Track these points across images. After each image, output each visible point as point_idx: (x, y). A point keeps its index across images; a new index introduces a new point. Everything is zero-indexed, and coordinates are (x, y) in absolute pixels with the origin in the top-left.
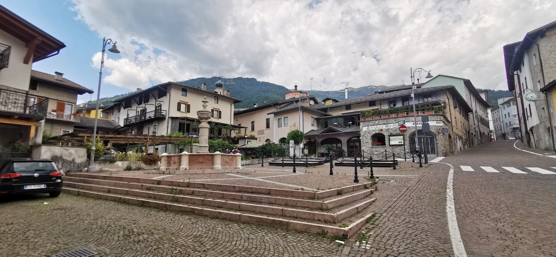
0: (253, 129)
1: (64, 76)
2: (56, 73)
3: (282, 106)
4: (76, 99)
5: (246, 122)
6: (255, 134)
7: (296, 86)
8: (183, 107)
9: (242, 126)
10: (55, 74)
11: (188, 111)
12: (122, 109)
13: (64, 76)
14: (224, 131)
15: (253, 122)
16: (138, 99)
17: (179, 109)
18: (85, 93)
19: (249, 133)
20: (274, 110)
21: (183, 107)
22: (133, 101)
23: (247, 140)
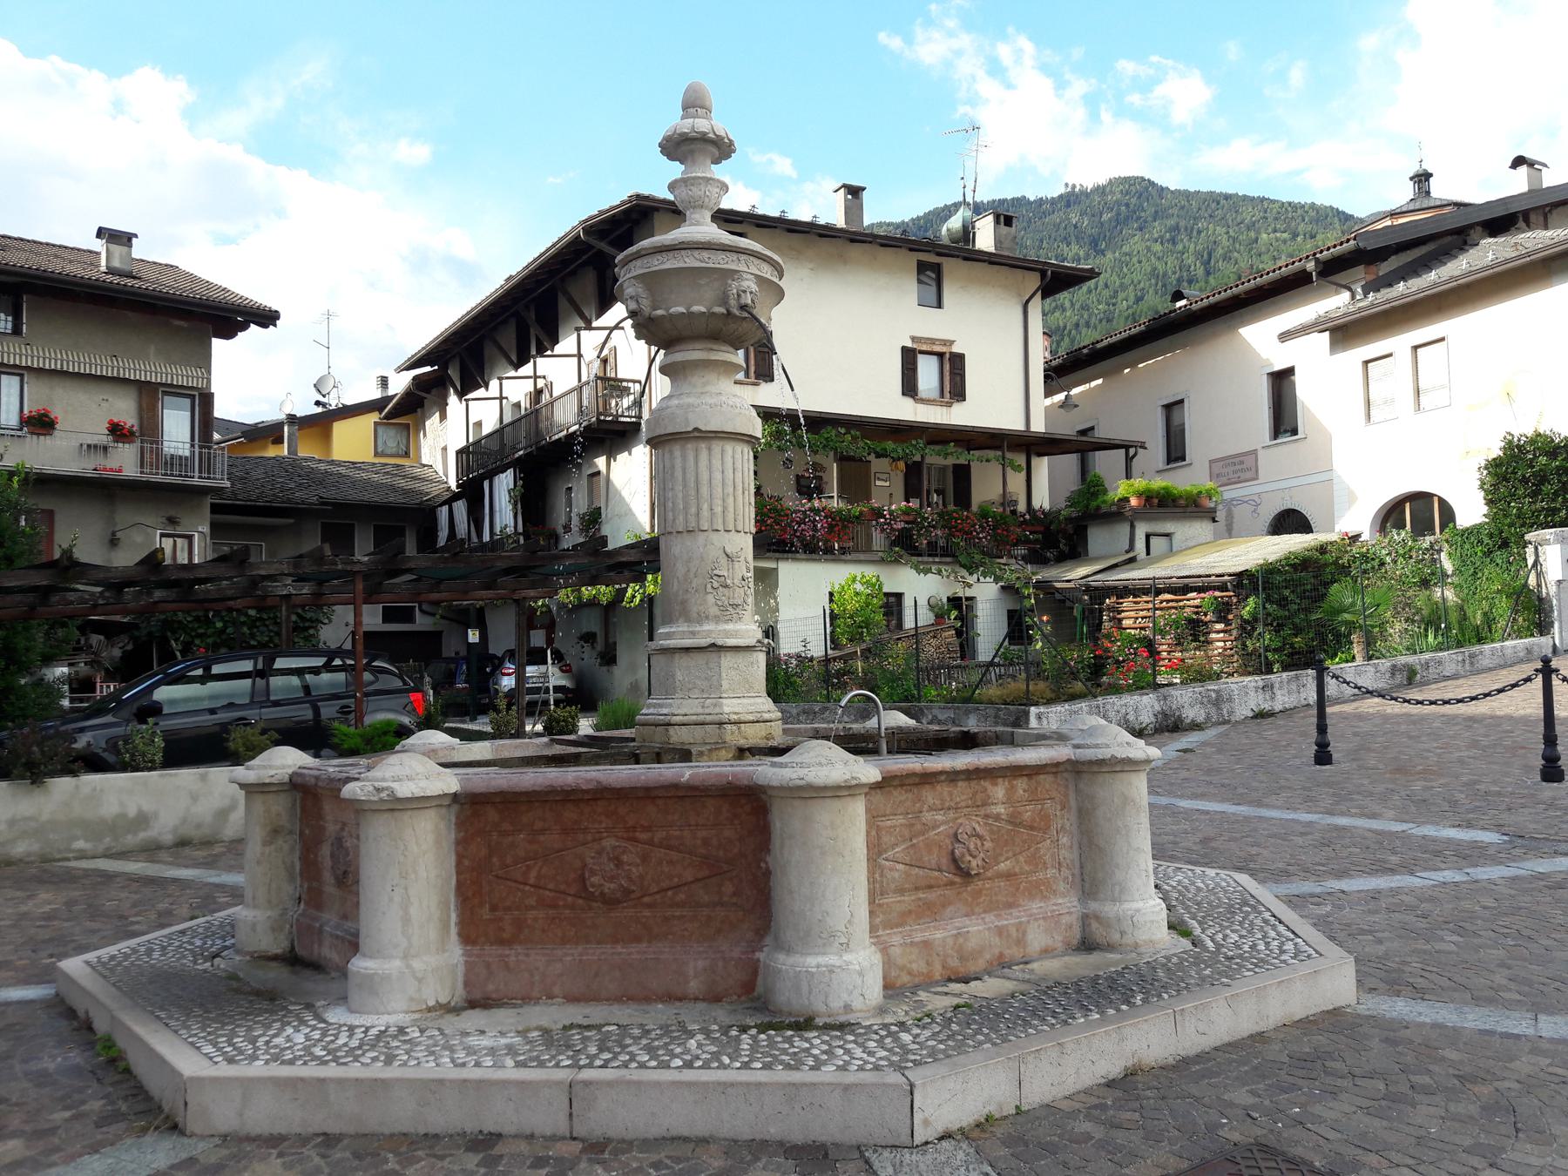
0: (1176, 452)
1: (139, 251)
2: (101, 233)
3: (1385, 268)
4: (205, 361)
5: (1120, 403)
6: (1189, 479)
7: (1422, 178)
8: (928, 373)
9: (1102, 433)
10: (99, 246)
11: (955, 388)
12: (453, 399)
13: (139, 251)
14: (988, 486)
15: (1172, 408)
16: (508, 337)
17: (909, 387)
18: (244, 327)
19: (1152, 476)
20: (1335, 303)
21: (928, 373)
22: (489, 350)
23: (1141, 530)
